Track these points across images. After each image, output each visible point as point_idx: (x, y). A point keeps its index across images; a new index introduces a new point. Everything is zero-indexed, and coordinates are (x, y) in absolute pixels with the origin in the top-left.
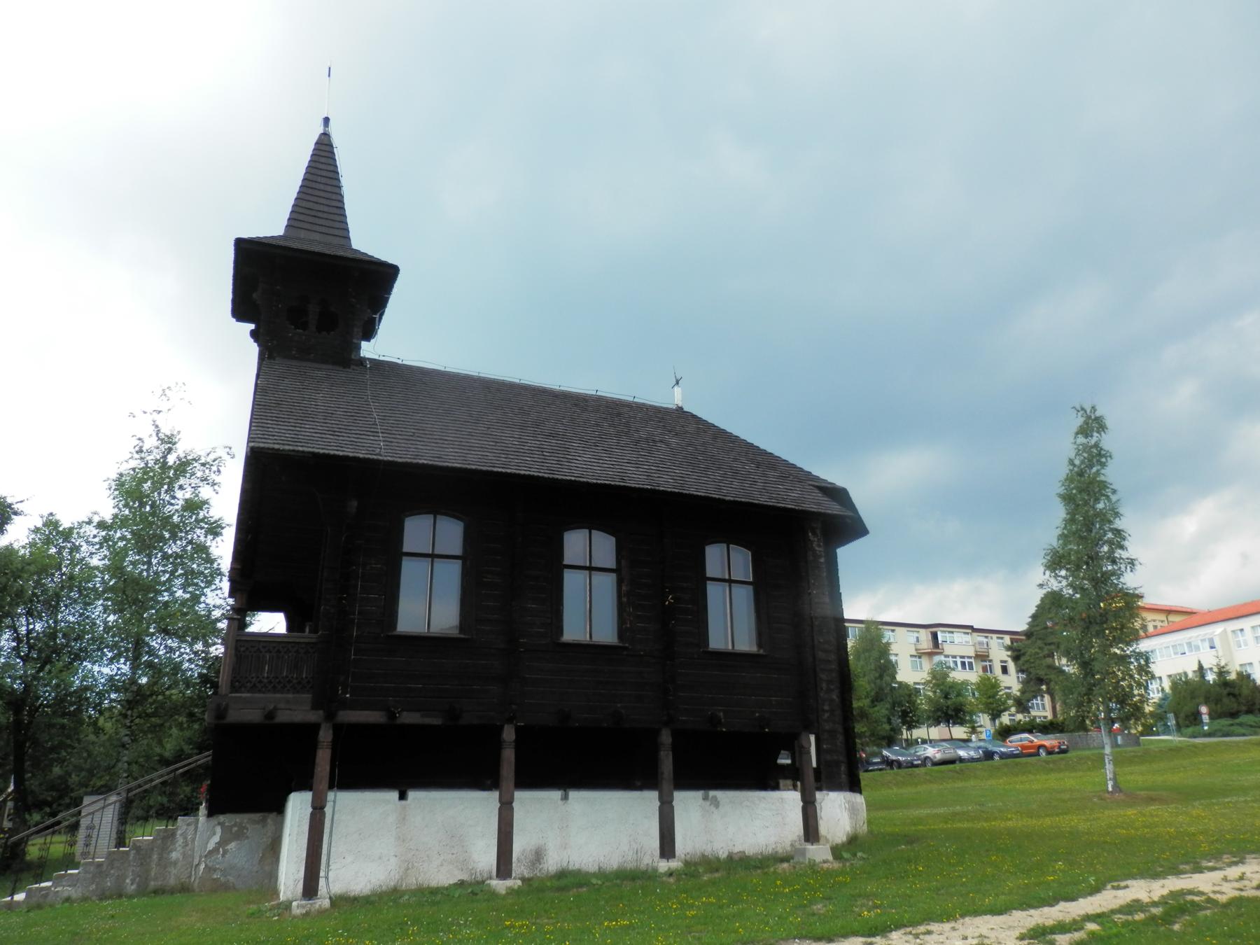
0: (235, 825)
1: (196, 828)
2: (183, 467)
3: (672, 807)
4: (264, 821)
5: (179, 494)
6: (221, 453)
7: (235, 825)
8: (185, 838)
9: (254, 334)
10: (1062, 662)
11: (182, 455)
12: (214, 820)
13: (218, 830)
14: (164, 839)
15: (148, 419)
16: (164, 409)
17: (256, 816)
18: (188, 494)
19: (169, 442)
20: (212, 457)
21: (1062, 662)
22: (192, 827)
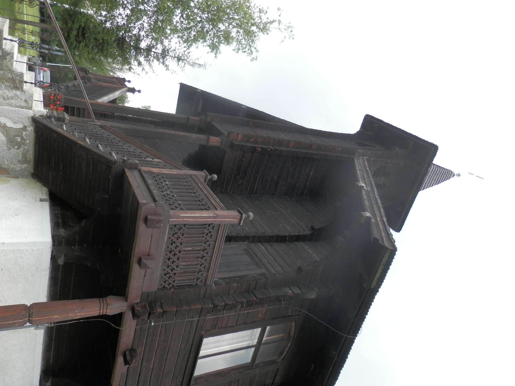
0: (22, 139)
1: (22, 107)
2: (249, 34)
3: (21, 325)
4: (24, 161)
5: (235, 30)
6: (254, 55)
7: (22, 139)
8: (12, 98)
9: (398, 229)
10: (65, 129)
11: (256, 35)
12: (28, 123)
13: (20, 126)
14: (13, 80)
15: (277, 18)
16: (281, 26)
17: (31, 156)
18: (233, 34)
19: (264, 29)
20: (253, 49)
21: (65, 129)
22: (23, 104)
